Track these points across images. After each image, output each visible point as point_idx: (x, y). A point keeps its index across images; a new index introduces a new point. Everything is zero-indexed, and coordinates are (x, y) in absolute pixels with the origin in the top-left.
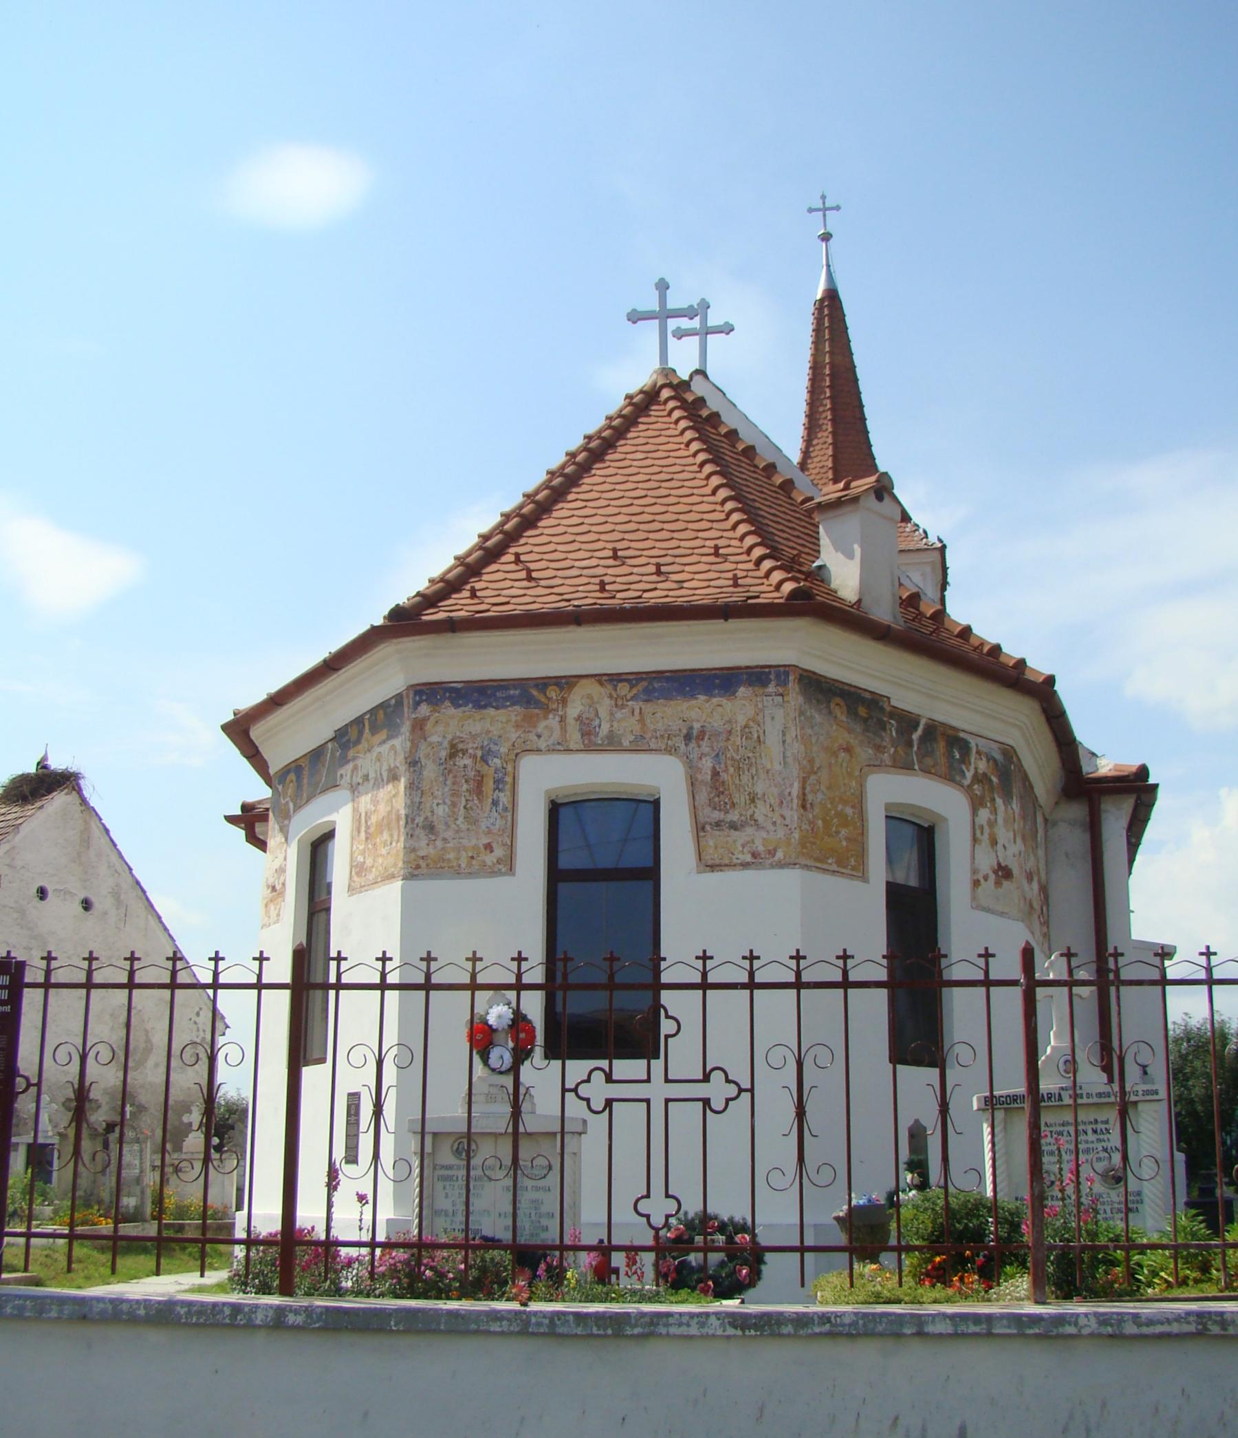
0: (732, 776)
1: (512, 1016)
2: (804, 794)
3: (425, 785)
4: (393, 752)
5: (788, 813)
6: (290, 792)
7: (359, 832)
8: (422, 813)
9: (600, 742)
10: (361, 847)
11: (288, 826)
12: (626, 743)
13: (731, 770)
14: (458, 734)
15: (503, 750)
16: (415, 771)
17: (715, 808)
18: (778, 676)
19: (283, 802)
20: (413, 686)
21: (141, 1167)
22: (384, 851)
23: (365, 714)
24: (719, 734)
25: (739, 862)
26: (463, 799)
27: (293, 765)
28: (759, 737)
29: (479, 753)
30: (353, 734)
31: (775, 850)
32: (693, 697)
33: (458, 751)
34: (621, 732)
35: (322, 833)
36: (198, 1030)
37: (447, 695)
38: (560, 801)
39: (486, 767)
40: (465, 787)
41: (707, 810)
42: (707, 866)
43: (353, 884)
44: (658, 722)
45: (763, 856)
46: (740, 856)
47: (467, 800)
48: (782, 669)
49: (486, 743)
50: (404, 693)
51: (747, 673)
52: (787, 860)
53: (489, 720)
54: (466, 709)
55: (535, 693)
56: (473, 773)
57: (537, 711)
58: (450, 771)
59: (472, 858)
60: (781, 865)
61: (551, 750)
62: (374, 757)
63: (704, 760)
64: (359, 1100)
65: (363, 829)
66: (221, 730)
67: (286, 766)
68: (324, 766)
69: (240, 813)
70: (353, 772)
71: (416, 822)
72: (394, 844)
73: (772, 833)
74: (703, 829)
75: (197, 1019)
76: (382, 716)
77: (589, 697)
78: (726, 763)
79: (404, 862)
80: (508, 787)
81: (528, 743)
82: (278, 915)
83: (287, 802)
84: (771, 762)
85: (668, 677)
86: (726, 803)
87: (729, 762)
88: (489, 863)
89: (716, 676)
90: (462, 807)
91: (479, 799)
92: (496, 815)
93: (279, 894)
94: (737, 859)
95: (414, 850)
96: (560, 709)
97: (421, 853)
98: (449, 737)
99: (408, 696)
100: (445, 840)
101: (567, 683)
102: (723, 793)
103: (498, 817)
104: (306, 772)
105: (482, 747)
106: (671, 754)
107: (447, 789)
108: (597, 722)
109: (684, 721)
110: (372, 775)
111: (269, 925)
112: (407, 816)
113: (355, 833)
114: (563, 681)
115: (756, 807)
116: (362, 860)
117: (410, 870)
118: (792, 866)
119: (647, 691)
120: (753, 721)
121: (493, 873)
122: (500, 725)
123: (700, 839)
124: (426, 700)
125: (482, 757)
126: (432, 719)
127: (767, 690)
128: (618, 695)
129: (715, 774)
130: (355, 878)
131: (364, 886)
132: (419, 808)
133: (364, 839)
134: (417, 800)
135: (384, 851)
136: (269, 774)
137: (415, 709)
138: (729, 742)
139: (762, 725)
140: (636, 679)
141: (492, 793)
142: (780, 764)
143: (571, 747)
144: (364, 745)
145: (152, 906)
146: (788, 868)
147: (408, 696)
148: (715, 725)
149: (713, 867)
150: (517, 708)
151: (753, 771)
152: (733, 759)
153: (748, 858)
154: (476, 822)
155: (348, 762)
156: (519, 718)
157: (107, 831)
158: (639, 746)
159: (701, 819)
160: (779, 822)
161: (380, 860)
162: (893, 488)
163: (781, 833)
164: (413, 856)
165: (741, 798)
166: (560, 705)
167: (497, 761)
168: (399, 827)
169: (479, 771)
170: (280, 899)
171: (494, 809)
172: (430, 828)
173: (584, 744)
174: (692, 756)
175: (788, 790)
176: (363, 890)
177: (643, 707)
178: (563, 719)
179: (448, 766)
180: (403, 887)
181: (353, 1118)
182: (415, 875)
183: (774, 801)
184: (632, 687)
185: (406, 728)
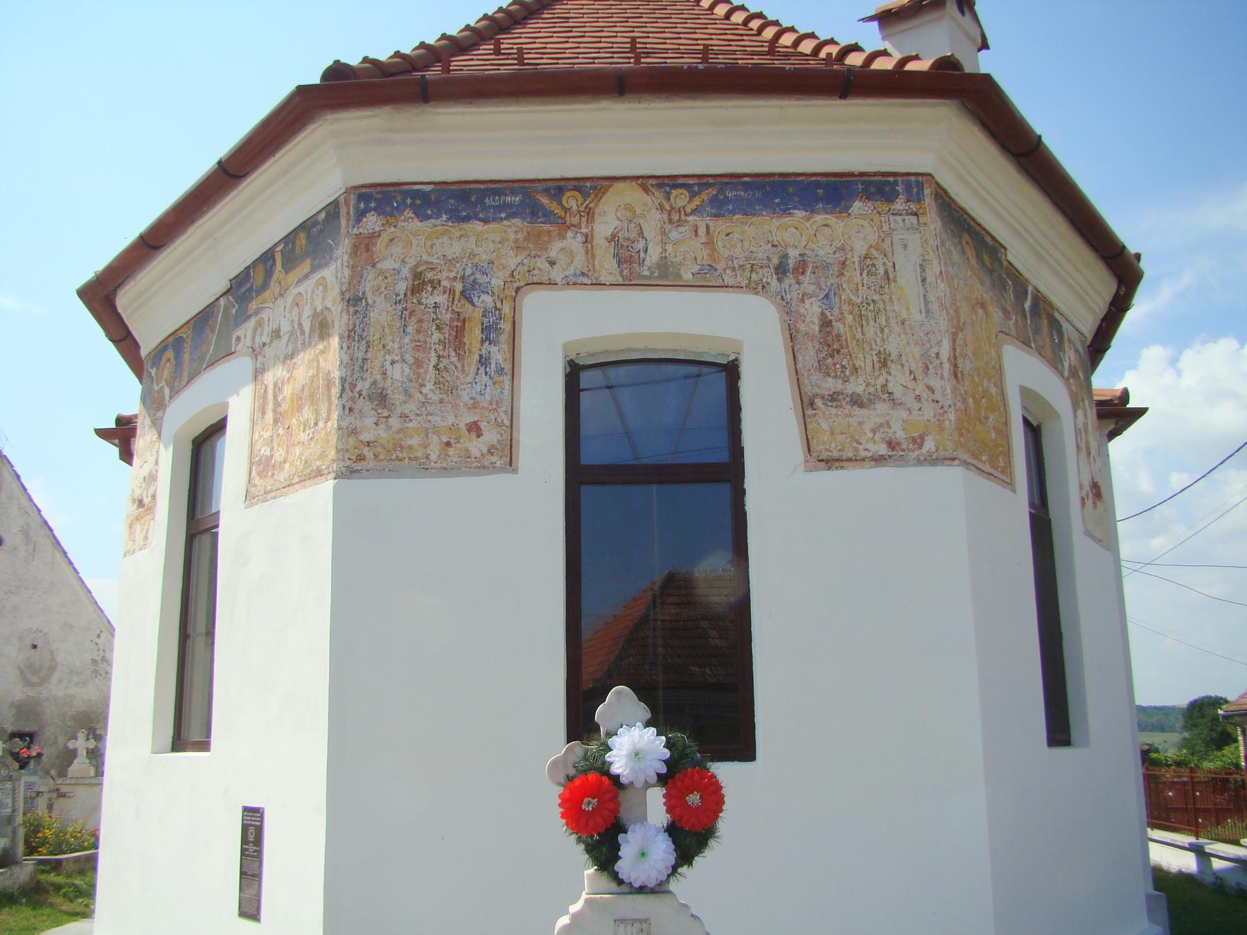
0: (851, 327)
1: (667, 753)
2: (955, 357)
3: (373, 334)
4: (321, 288)
5: (936, 383)
6: (166, 374)
7: (263, 413)
8: (367, 375)
9: (647, 273)
10: (267, 435)
11: (162, 418)
12: (687, 276)
13: (850, 318)
14: (425, 257)
15: (497, 282)
16: (356, 312)
17: (829, 375)
18: (908, 188)
19: (157, 388)
20: (356, 188)
21: (13, 806)
22: (303, 437)
23: (276, 245)
24: (827, 267)
25: (870, 454)
26: (433, 354)
27: (171, 339)
28: (886, 272)
29: (459, 287)
30: (258, 277)
31: (922, 440)
32: (786, 212)
33: (424, 283)
34: (679, 259)
35: (209, 425)
36: (99, 650)
37: (409, 201)
38: (581, 363)
39: (468, 306)
40: (436, 336)
41: (816, 377)
42: (819, 461)
43: (253, 489)
44: (734, 246)
45: (904, 447)
46: (870, 446)
47: (439, 357)
48: (913, 179)
49: (469, 272)
50: (342, 200)
51: (863, 183)
52: (942, 453)
53: (473, 239)
54: (439, 222)
55: (544, 200)
56: (449, 316)
57: (547, 227)
58: (412, 313)
59: (448, 444)
60: (933, 460)
61: (570, 284)
62: (289, 304)
63: (807, 302)
64: (262, 821)
65: (270, 406)
66: (76, 295)
67: (163, 341)
68: (213, 331)
69: (114, 426)
70: (255, 330)
71: (358, 389)
72: (321, 424)
73: (915, 412)
74: (812, 404)
75: (98, 641)
76: (304, 241)
77: (629, 208)
78: (840, 308)
79: (338, 451)
80: (504, 337)
81: (536, 272)
82: (146, 538)
83: (162, 387)
84: (908, 309)
85: (745, 184)
86: (843, 367)
87: (845, 307)
88: (475, 452)
89: (818, 185)
90: (431, 368)
91: (458, 355)
92: (485, 379)
93: (147, 510)
94: (866, 450)
95: (354, 432)
96: (583, 224)
97: (366, 437)
98: (411, 262)
99: (347, 203)
100: (404, 416)
101: (594, 188)
102: (838, 352)
103: (490, 383)
104: (187, 346)
105: (463, 278)
106: (757, 293)
107: (407, 340)
108: (641, 245)
109: (773, 246)
110: (285, 328)
111: (134, 552)
112: (343, 380)
113: (258, 415)
114: (588, 184)
115: (889, 373)
116: (268, 453)
117: (348, 463)
118: (948, 462)
119: (714, 201)
120: (877, 250)
121: (483, 468)
122: (491, 246)
123: (808, 420)
124: (375, 209)
125: (463, 293)
126: (385, 237)
127: (893, 207)
128: (671, 206)
129: (826, 323)
130: (257, 481)
131: (271, 491)
132: (362, 368)
133: (271, 422)
134: (360, 355)
135: (303, 437)
136: (139, 356)
137: (359, 220)
138: (844, 279)
139: (890, 254)
140: (699, 185)
141: (478, 346)
142: (921, 312)
143: (603, 279)
144: (274, 287)
145: (58, 543)
146: (943, 465)
147: (347, 203)
148: (821, 253)
149: (830, 463)
150: (517, 221)
151: (882, 319)
152: (850, 302)
153: (883, 449)
154: (452, 390)
155: (249, 317)
156: (520, 236)
157: (18, 477)
158: (708, 280)
159: (808, 390)
160: (925, 395)
161: (298, 451)
162: (974, 5)
163: (929, 412)
164: (352, 441)
165: (865, 361)
166: (584, 219)
167: (487, 299)
168: (329, 397)
169: (458, 314)
170: (148, 517)
171: (482, 370)
172: (381, 398)
173: (622, 276)
174: (788, 296)
175: (935, 350)
176: (269, 497)
177: (711, 224)
178: (588, 239)
179: (409, 305)
180: (337, 493)
181: (251, 847)
182: (357, 471)
183: (916, 366)
184: (692, 197)
185: (343, 250)
